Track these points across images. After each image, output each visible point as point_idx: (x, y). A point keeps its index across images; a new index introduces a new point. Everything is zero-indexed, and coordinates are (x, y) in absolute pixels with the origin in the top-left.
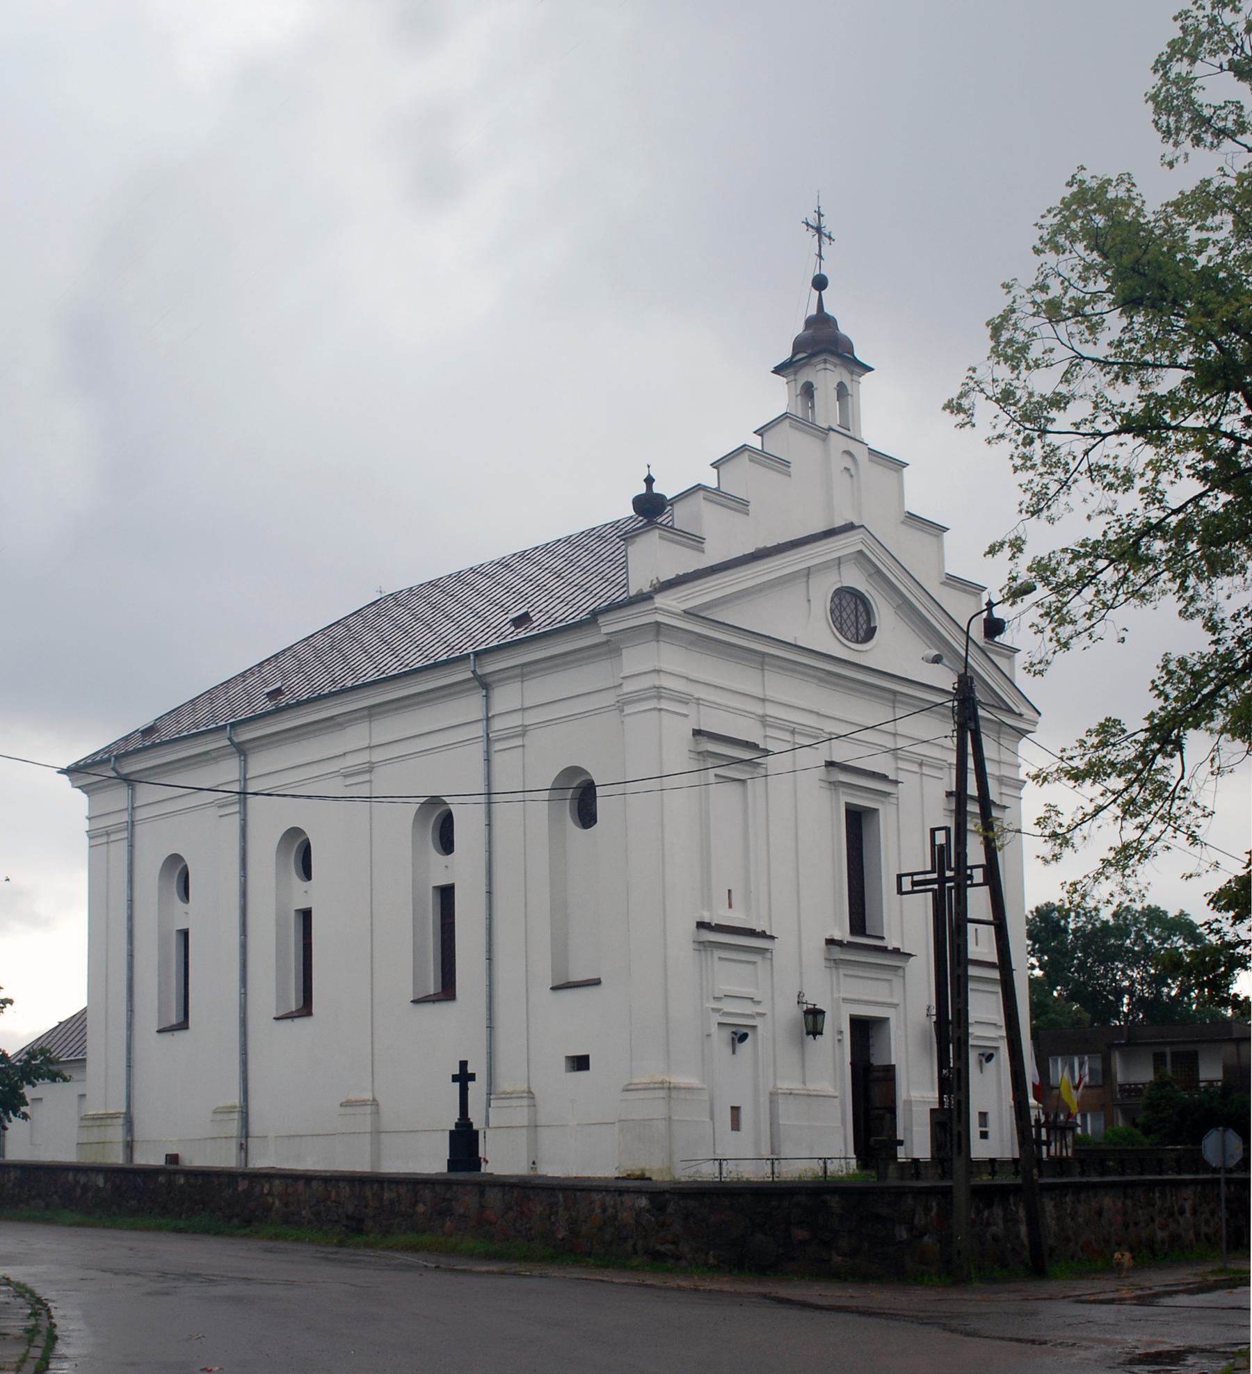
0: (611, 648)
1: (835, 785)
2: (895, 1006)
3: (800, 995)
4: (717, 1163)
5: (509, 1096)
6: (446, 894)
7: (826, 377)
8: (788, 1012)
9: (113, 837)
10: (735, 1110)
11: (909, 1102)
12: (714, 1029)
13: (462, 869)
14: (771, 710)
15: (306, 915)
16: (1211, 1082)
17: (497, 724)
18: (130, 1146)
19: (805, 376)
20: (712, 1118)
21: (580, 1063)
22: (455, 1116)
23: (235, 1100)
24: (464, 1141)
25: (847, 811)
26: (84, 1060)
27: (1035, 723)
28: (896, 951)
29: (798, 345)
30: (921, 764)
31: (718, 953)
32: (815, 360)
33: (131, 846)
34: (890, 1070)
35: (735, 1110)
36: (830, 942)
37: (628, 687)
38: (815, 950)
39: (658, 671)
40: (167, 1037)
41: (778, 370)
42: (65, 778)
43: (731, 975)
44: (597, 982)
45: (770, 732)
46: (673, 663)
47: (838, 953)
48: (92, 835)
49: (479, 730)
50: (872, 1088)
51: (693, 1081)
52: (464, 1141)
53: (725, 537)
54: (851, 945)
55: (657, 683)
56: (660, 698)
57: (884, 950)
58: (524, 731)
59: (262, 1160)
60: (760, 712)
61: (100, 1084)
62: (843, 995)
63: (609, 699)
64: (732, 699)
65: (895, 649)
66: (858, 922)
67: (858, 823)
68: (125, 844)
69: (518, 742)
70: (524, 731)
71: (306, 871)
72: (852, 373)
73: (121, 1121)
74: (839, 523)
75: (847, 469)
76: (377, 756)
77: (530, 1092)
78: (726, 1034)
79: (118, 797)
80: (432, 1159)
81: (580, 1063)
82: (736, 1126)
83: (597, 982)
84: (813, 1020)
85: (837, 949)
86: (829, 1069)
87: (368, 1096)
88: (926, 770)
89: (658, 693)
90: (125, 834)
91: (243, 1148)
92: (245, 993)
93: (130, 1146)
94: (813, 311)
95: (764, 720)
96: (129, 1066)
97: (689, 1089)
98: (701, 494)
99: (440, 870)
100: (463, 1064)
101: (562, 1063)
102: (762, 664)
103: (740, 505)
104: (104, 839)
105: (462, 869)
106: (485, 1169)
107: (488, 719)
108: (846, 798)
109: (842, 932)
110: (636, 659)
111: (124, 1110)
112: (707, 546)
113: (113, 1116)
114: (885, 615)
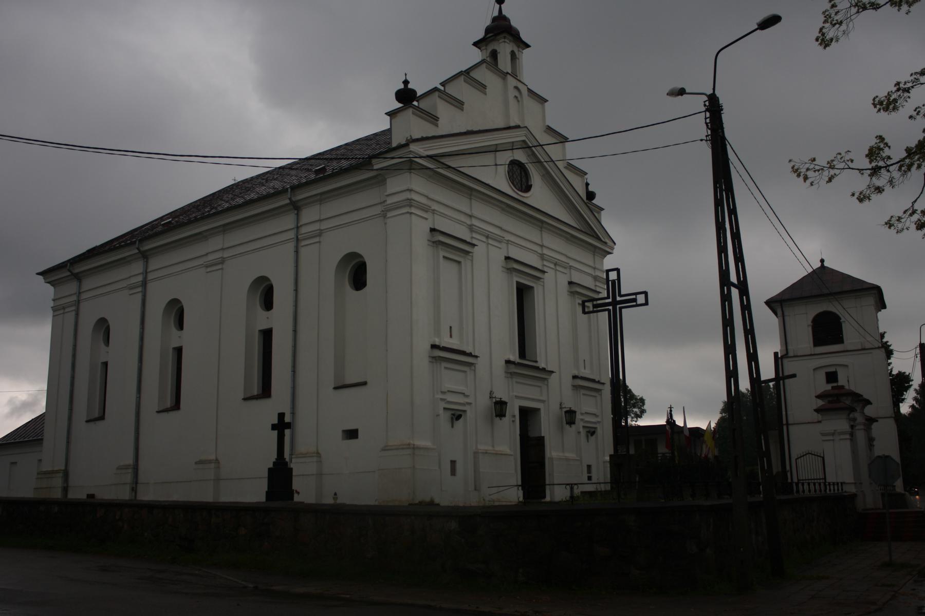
0: (380, 180)
1: (510, 270)
2: (543, 401)
3: (491, 393)
4: (568, 487)
5: (305, 455)
6: (267, 335)
7: (505, 48)
8: (483, 402)
9: (67, 310)
10: (453, 463)
11: (551, 459)
12: (441, 412)
13: (279, 319)
14: (546, 251)
15: (179, 351)
16: (663, 454)
17: (303, 230)
18: (65, 490)
19: (491, 47)
20: (440, 467)
21: (352, 434)
22: (274, 456)
23: (130, 461)
24: (280, 476)
25: (517, 288)
26: (42, 439)
27: (613, 249)
28: (544, 369)
29: (488, 30)
30: (555, 264)
31: (444, 364)
32: (498, 37)
33: (77, 315)
34: (541, 439)
35: (453, 463)
36: (508, 362)
37: (390, 201)
38: (499, 364)
39: (410, 190)
40: (92, 424)
41: (476, 44)
42: (41, 277)
43: (451, 380)
44: (365, 383)
45: (474, 235)
46: (420, 186)
47: (513, 369)
48: (55, 309)
49: (292, 235)
50: (532, 451)
51: (427, 443)
52: (280, 476)
53: (450, 120)
54: (519, 364)
55: (409, 197)
56: (411, 206)
57: (537, 368)
58: (320, 233)
59: (147, 495)
60: (469, 222)
61: (51, 454)
62: (515, 394)
63: (378, 210)
64: (454, 213)
65: (540, 196)
66: (522, 354)
67: (523, 293)
68: (74, 313)
69: (317, 240)
70: (320, 233)
71: (180, 325)
72: (518, 47)
73: (61, 475)
74: (512, 124)
75: (516, 97)
76: (226, 254)
77: (318, 453)
78: (449, 414)
79: (71, 288)
80: (254, 492)
81: (352, 434)
82: (453, 472)
83: (365, 383)
84: (500, 408)
85: (513, 366)
86: (506, 439)
87: (213, 457)
88: (558, 268)
89: (410, 203)
90: (73, 308)
91: (134, 490)
92: (140, 397)
93: (65, 490)
94: (496, 14)
95: (471, 228)
96: (68, 442)
97: (426, 449)
98: (437, 93)
99: (263, 320)
100: (281, 416)
101: (340, 434)
102: (471, 195)
103: (459, 104)
104: (61, 312)
105: (279, 319)
106: (297, 498)
107: (298, 227)
108: (516, 278)
109: (514, 357)
110: (396, 184)
111: (63, 468)
112: (440, 122)
113: (57, 472)
114: (536, 180)
